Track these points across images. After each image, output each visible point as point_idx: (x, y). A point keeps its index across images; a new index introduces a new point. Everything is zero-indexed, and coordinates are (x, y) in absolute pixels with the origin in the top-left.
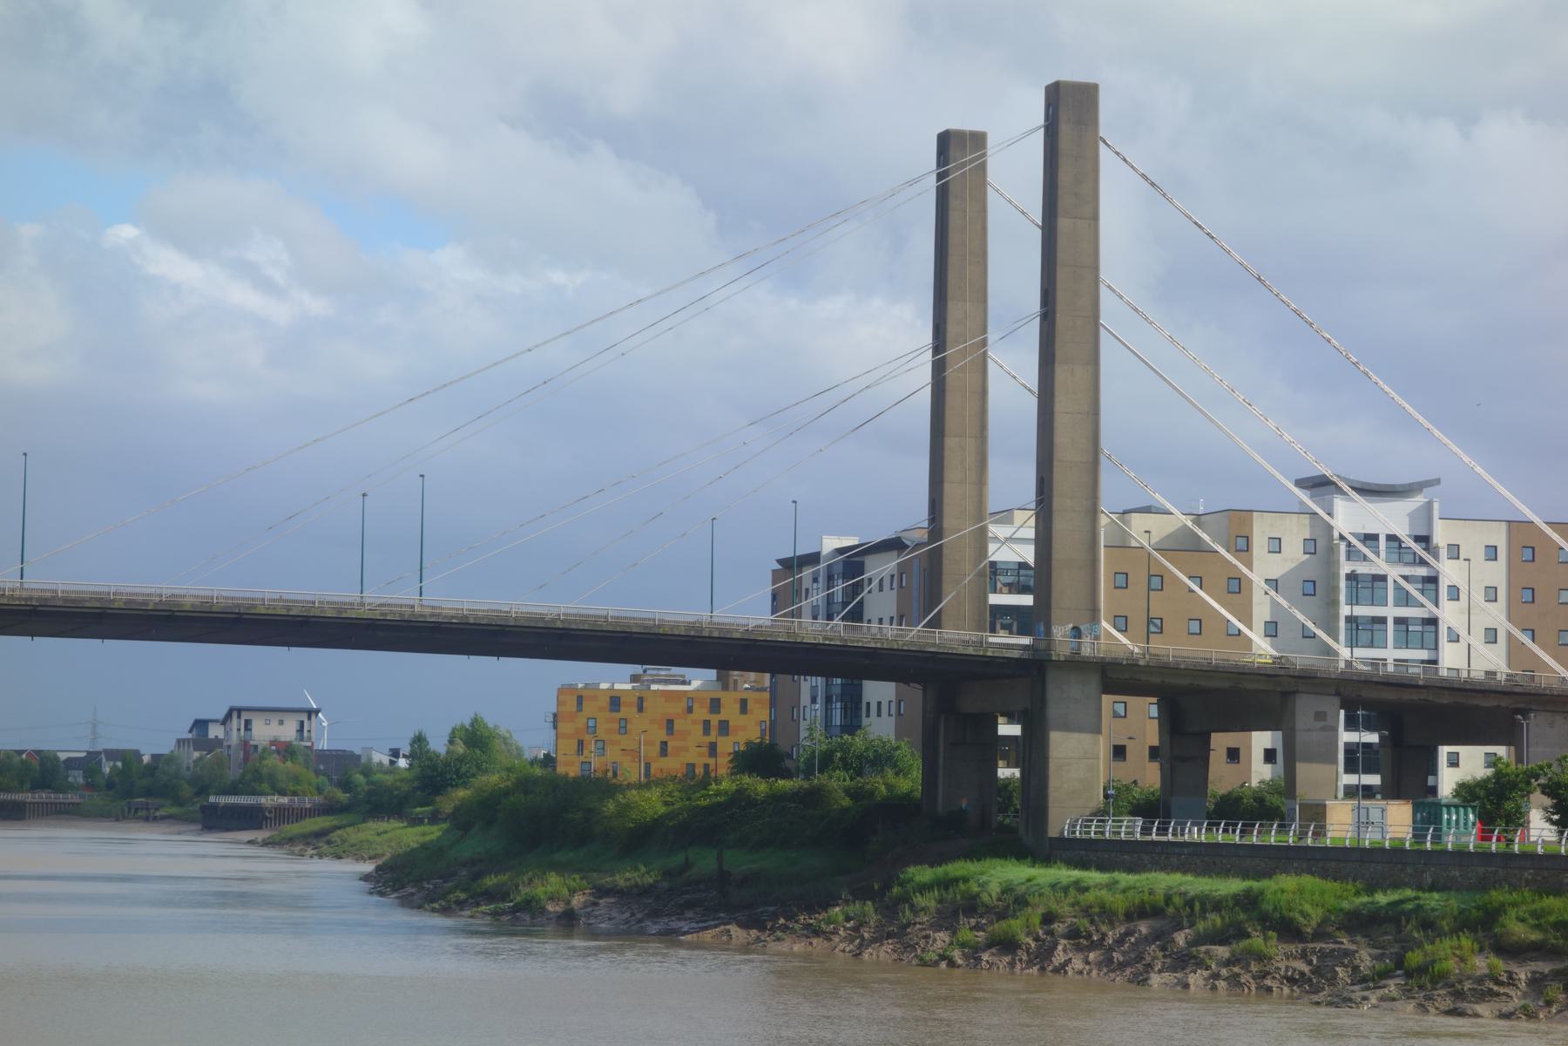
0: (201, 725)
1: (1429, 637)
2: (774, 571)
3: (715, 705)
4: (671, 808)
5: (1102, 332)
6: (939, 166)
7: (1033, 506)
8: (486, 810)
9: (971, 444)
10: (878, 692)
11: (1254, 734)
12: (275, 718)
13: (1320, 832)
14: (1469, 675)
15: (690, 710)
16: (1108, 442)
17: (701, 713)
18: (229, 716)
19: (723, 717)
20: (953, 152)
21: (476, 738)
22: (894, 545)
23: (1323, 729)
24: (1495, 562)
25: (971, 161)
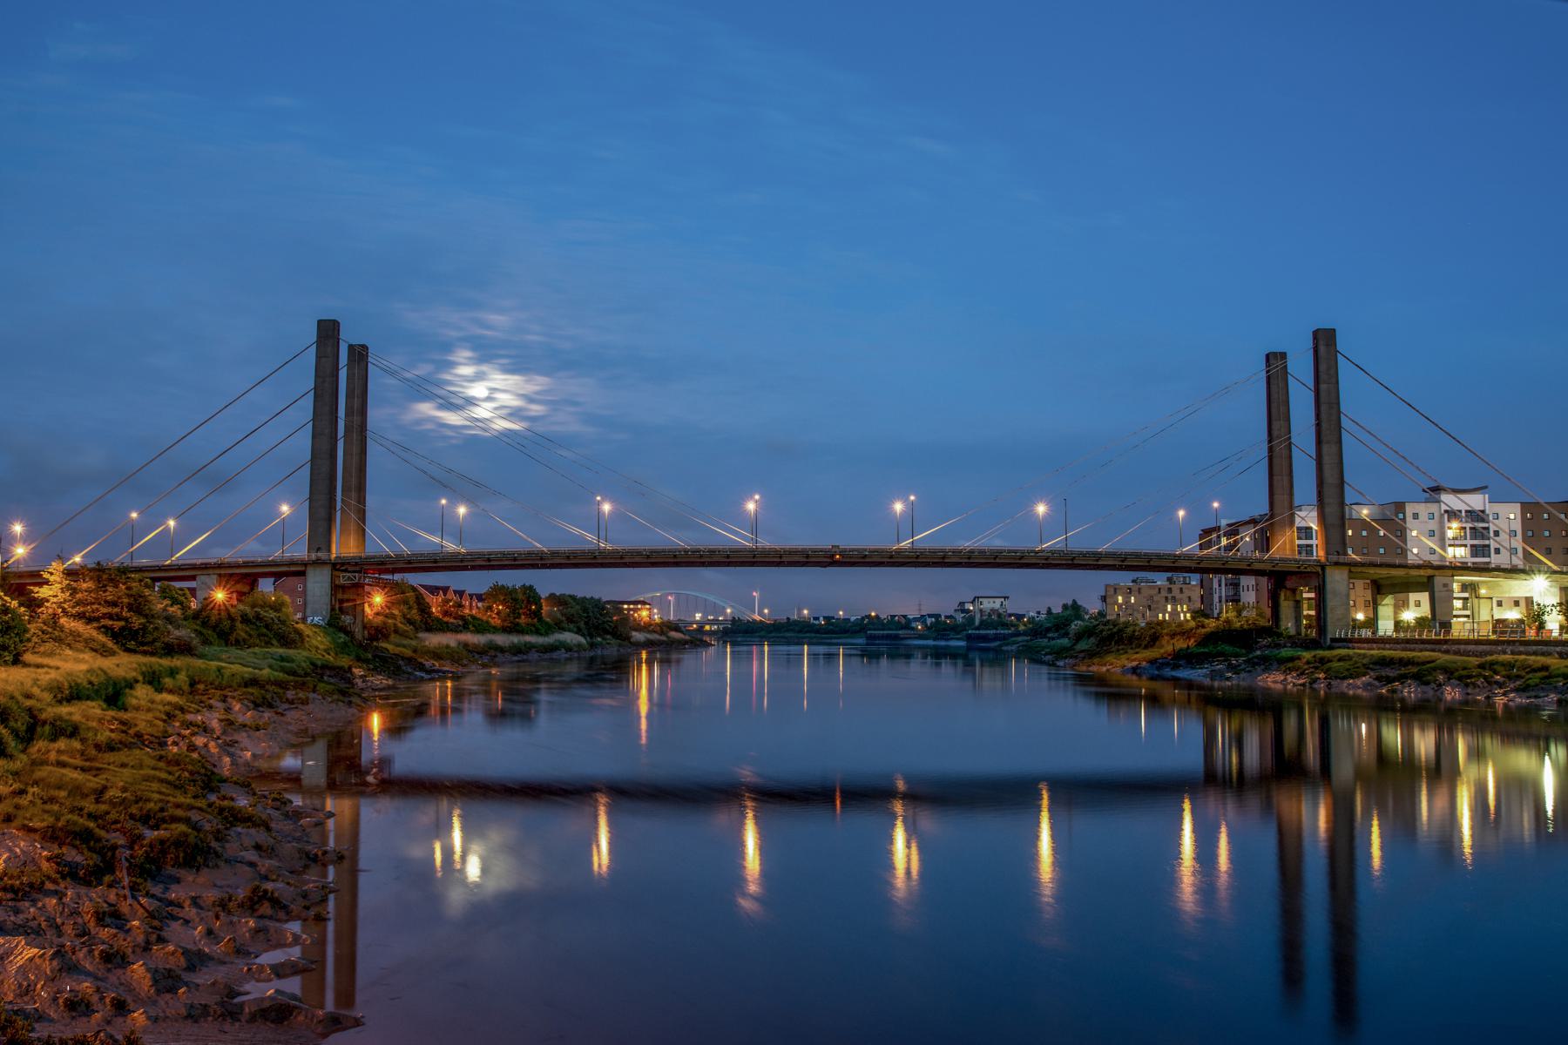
0: (962, 604)
1: (1486, 552)
2: (1200, 535)
3: (1170, 590)
4: (113, 908)
5: (1343, 431)
6: (1267, 366)
7: (1315, 503)
8: (1087, 633)
9: (1286, 479)
10: (1247, 581)
11: (1410, 594)
12: (992, 600)
13: (1448, 632)
14: (1455, 598)
15: (1160, 592)
16: (369, 427)
17: (1164, 593)
18: (974, 600)
19: (1173, 595)
20: (1272, 361)
21: (1075, 609)
22: (1253, 522)
23: (1447, 591)
24: (1108, 583)
25: (1281, 364)
